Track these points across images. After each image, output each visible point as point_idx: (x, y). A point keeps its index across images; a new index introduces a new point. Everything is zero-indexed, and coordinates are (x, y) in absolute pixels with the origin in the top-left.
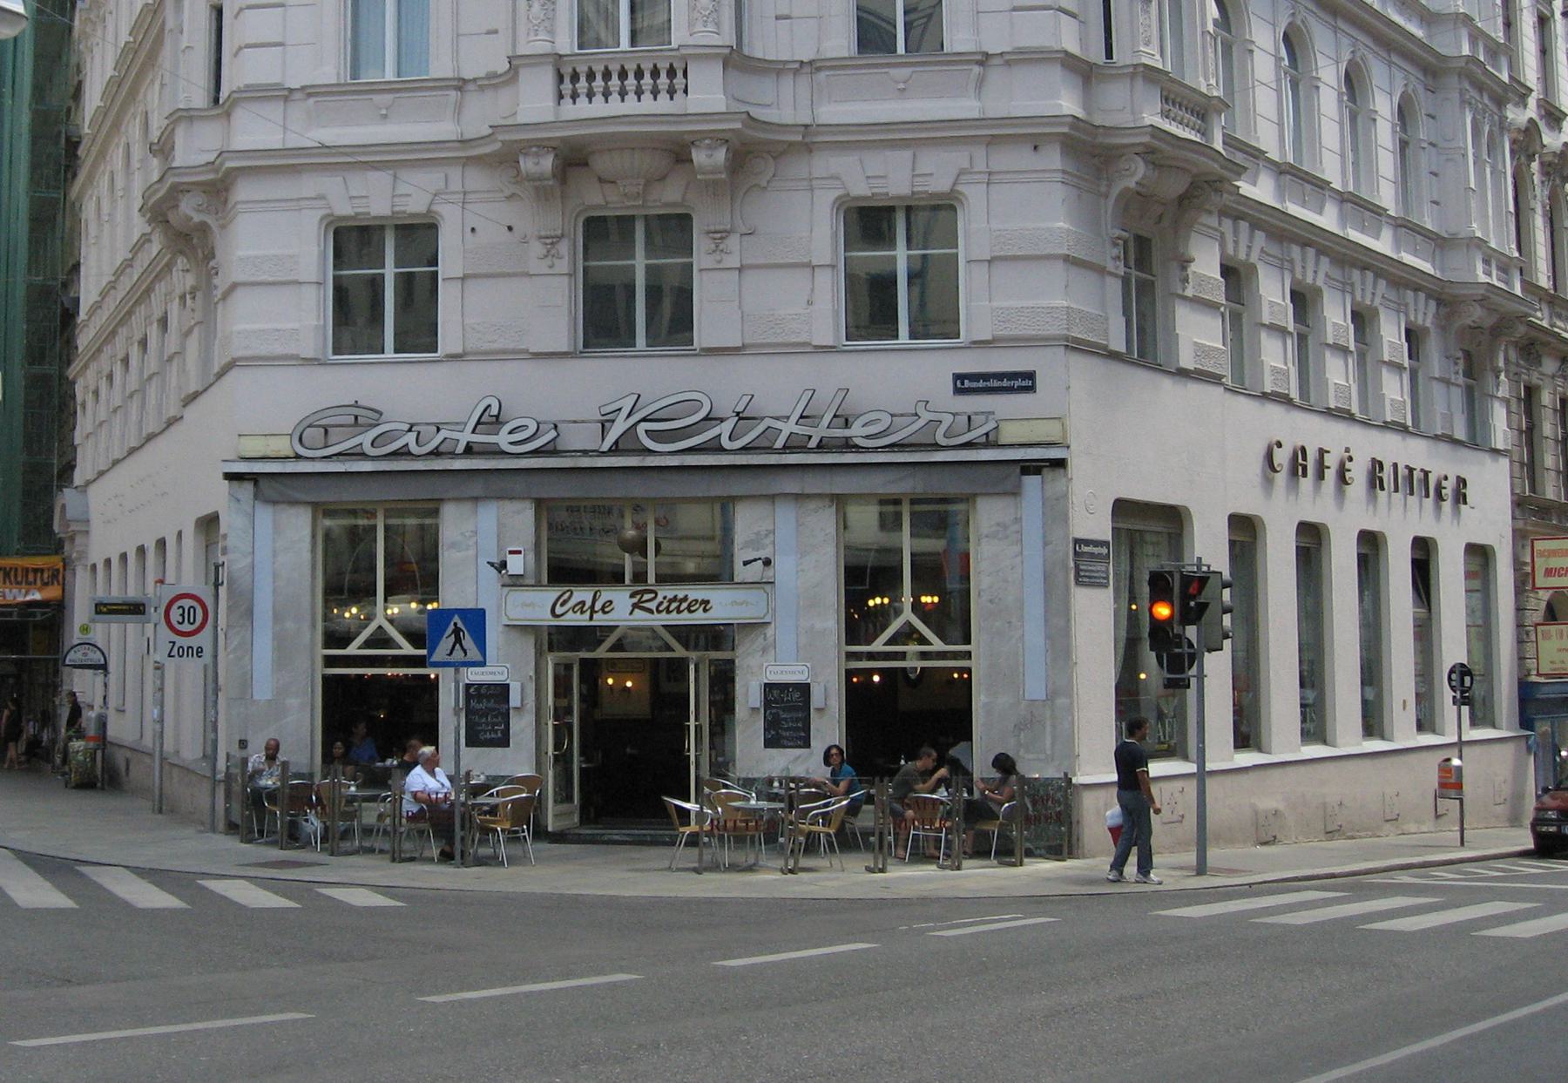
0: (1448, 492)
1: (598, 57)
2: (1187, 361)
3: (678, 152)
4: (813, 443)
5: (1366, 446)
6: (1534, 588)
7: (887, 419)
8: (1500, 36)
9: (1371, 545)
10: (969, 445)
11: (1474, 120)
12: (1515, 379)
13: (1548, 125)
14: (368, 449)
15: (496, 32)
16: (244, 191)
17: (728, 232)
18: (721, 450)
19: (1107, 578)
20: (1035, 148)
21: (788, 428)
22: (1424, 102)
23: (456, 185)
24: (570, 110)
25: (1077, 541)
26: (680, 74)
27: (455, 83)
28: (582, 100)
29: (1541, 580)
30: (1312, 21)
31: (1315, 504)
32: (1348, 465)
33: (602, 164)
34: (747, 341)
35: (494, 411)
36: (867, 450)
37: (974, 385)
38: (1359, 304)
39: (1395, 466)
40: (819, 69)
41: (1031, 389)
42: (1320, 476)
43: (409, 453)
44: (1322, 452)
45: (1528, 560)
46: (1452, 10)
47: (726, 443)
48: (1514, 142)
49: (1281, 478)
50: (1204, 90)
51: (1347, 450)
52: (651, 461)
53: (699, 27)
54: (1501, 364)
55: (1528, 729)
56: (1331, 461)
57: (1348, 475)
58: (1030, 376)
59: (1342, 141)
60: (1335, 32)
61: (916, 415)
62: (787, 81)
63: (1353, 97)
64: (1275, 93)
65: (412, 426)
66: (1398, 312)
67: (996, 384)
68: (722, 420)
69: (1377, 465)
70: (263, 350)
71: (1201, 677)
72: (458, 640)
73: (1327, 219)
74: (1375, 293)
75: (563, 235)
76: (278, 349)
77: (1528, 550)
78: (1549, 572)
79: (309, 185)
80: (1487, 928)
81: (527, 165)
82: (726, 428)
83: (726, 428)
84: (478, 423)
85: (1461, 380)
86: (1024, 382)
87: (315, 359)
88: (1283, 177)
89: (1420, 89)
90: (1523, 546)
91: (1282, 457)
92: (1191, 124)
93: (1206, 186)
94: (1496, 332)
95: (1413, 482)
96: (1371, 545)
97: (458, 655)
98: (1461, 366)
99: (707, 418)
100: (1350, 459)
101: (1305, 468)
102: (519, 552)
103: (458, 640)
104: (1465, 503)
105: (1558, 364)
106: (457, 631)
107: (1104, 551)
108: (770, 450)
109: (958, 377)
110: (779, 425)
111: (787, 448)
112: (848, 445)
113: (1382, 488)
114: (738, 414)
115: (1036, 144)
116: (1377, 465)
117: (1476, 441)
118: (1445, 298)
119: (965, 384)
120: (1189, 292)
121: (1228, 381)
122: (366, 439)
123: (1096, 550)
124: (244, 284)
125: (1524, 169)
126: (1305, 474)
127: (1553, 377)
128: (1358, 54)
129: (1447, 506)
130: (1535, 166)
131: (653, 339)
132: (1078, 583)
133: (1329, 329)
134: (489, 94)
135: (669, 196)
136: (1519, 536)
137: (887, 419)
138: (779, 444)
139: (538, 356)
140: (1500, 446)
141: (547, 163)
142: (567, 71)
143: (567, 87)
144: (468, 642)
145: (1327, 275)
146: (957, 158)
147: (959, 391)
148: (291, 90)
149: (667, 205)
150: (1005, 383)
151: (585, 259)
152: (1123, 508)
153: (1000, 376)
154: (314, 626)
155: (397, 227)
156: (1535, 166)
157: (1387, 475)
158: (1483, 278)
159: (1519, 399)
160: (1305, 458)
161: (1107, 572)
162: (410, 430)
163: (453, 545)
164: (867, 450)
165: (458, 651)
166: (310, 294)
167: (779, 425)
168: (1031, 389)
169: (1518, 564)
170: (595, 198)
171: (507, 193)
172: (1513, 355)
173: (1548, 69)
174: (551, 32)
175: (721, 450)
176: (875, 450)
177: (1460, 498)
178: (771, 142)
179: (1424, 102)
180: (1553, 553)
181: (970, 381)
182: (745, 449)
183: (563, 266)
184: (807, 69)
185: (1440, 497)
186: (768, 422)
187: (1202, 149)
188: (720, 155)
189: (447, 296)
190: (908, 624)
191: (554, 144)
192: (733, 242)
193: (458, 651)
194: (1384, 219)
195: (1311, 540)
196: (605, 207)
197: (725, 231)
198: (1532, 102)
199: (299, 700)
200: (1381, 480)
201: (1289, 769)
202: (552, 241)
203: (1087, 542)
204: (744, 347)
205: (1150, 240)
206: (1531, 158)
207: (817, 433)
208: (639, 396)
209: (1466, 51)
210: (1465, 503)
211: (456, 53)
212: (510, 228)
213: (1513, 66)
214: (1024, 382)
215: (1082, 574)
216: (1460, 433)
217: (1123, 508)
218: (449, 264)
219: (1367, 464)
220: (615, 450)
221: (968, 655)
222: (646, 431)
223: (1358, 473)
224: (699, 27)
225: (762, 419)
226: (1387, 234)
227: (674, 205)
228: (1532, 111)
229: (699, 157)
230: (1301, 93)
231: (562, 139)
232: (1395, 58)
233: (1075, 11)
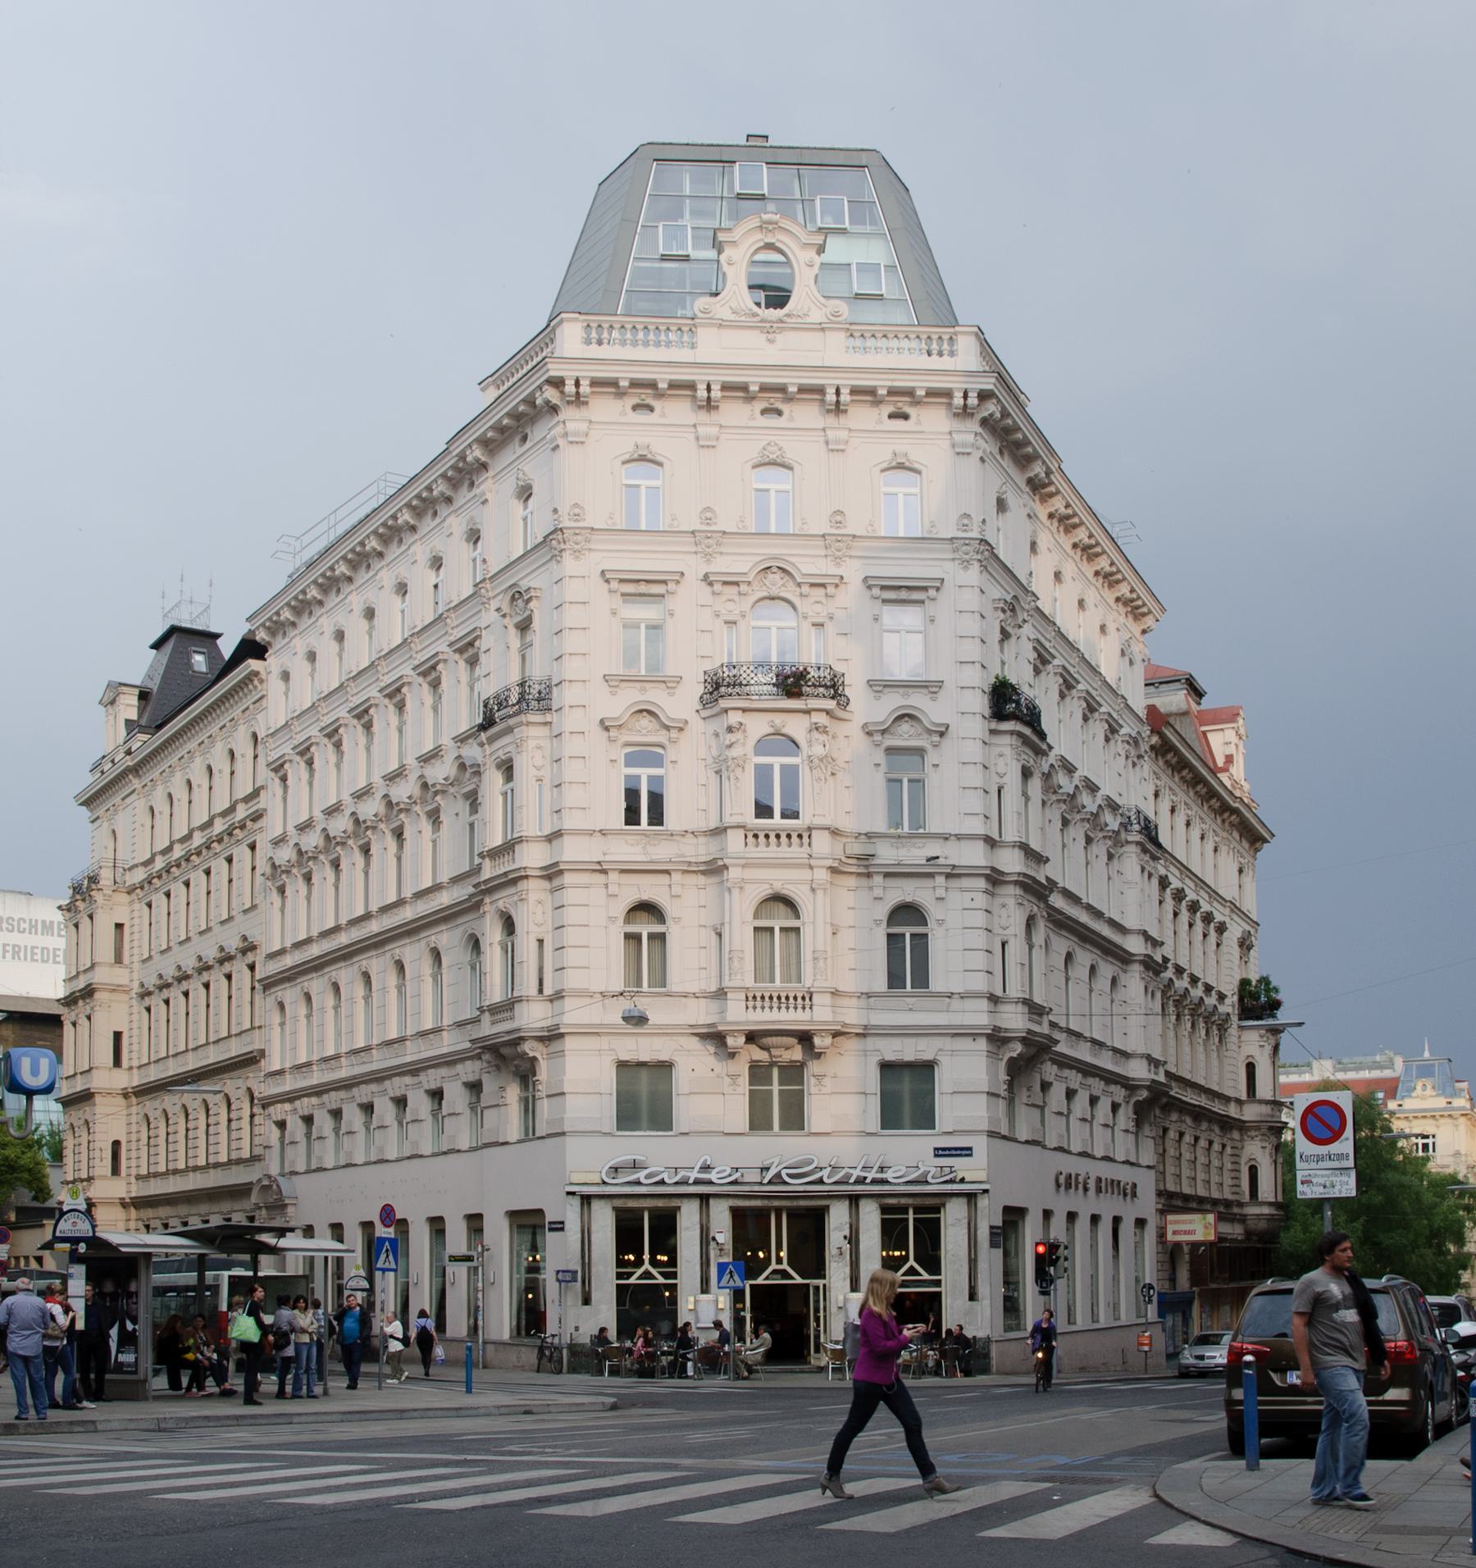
0: (1129, 1191)
1: (765, 987)
7: (904, 1169)
10: (951, 1181)
14: (643, 1180)
21: (856, 1173)
26: (807, 999)
36: (895, 1184)
41: (971, 1155)
42: (1077, 1188)
49: (1062, 1189)
56: (1081, 1179)
58: (970, 1149)
67: (954, 1152)
69: (1099, 1180)
71: (1055, 1290)
78: (1175, 1233)
80: (827, 1522)
91: (1062, 1179)
97: (387, 1265)
106: (731, 1272)
108: (847, 1183)
109: (936, 1149)
110: (851, 1171)
112: (884, 1182)
115: (974, 1036)
116: (1099, 1180)
119: (939, 1152)
122: (641, 1175)
129: (1129, 1198)
131: (782, 1128)
137: (904, 1169)
138: (852, 1181)
143: (751, 1004)
146: (938, 1043)
147: (936, 1156)
153: (950, 1149)
163: (687, 1228)
164: (895, 1184)
165: (732, 1282)
167: (851, 1171)
176: (899, 1184)
177: (1134, 1195)
182: (835, 1183)
185: (1125, 1195)
186: (846, 1170)
190: (912, 1267)
193: (732, 1282)
201: (1114, 1331)
202: (734, 1077)
207: (870, 1176)
220: (770, 1183)
221: (938, 1283)
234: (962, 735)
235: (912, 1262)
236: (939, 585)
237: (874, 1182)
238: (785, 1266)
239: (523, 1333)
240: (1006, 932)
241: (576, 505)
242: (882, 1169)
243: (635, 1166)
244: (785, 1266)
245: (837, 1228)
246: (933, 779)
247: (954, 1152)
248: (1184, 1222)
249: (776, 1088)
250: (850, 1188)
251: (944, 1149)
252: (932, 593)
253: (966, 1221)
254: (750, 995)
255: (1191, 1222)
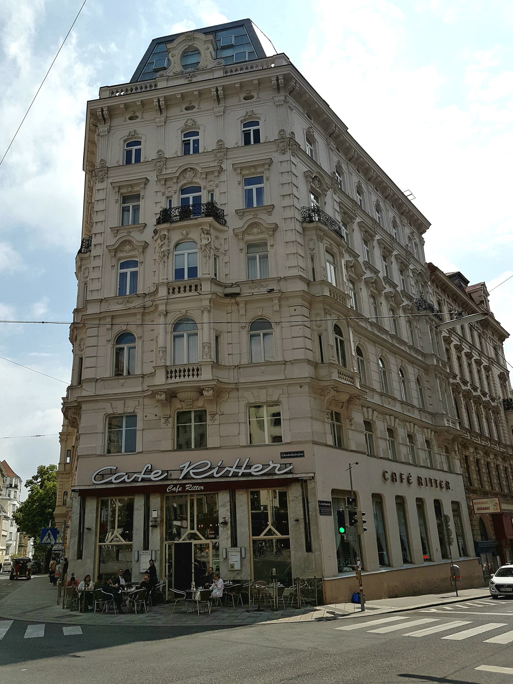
2: (353, 447)
3: (200, 391)
4: (240, 474)
5: (415, 472)
6: (475, 514)
8: (446, 360)
9: (420, 503)
11: (440, 382)
12: (461, 453)
13: (464, 384)
14: (114, 481)
15: (153, 362)
16: (84, 407)
17: (216, 414)
18: (214, 477)
19: (331, 513)
20: (301, 387)
21: (233, 470)
22: (424, 377)
23: (141, 403)
24: (170, 381)
25: (319, 502)
27: (141, 376)
28: (173, 378)
29: (476, 511)
30: (407, 365)
31: (401, 489)
32: (410, 478)
33: (181, 396)
34: (221, 445)
35: (150, 468)
37: (287, 455)
38: (366, 418)
39: (426, 478)
40: (240, 368)
41: (303, 456)
43: (126, 482)
44: (401, 475)
45: (472, 505)
46: (431, 353)
47: (215, 475)
48: (453, 389)
50: (352, 371)
51: (410, 474)
52: (195, 481)
53: (205, 357)
54: (457, 449)
55: (478, 557)
56: (405, 477)
57: (411, 481)
58: (302, 452)
59: (418, 395)
60: (396, 358)
61: (269, 465)
62: (231, 371)
63: (419, 385)
64: (416, 392)
65: (127, 473)
66: (422, 434)
67: (293, 455)
68: (214, 468)
70: (86, 453)
72: (49, 537)
73: (398, 408)
74: (410, 427)
75: (170, 417)
76: (90, 453)
77: (471, 502)
79: (100, 405)
81: (158, 397)
82: (215, 471)
83: (215, 471)
84: (145, 472)
85: (444, 454)
86: (300, 454)
87: (101, 455)
88: (382, 397)
89: (424, 374)
90: (470, 502)
91: (388, 476)
92: (347, 379)
93: (355, 397)
94: (454, 440)
95: (431, 482)
96: (420, 503)
98: (444, 450)
99: (210, 468)
100: (411, 476)
101: (396, 479)
102: (156, 510)
103: (49, 537)
104: (450, 489)
105: (474, 449)
106: (49, 534)
107: (329, 504)
108: (228, 477)
111: (233, 476)
112: (250, 475)
113: (422, 485)
114: (219, 466)
117: (451, 471)
118: (437, 431)
119: (284, 455)
120: (353, 428)
121: (367, 453)
123: (326, 504)
124: (82, 434)
125: (458, 396)
126: (396, 481)
127: (473, 453)
128: (403, 364)
130: (461, 395)
132: (321, 515)
133: (379, 432)
134: (150, 378)
135: (200, 404)
136: (468, 498)
138: (230, 475)
139: (162, 451)
140: (459, 473)
141: (163, 397)
142: (169, 370)
143: (169, 375)
144: (52, 537)
145: (398, 424)
148: (97, 379)
149: (199, 407)
150: (295, 455)
151: (177, 424)
152: (334, 491)
154: (96, 535)
155: (127, 417)
156: (461, 395)
157: (423, 481)
158: (447, 425)
159: (463, 459)
160: (396, 476)
161: (331, 511)
162: (126, 475)
166: (100, 436)
167: (230, 469)
168: (303, 456)
169: (469, 507)
170: (178, 406)
171: (155, 405)
172: (460, 446)
173: (482, 383)
174: (165, 360)
175: (214, 477)
177: (448, 488)
178: (226, 388)
179: (424, 377)
180: (479, 503)
181: (285, 454)
182: (221, 477)
183: (170, 425)
184: (237, 368)
185: (441, 488)
186: (227, 468)
187: (353, 387)
188: (211, 392)
189: (139, 435)
191: (166, 390)
192: (217, 416)
194: (415, 409)
195: (401, 501)
196: (182, 408)
197: (215, 414)
198: (479, 390)
199: (31, 558)
200: (422, 483)
202: (167, 418)
203: (323, 502)
204: (220, 447)
205: (340, 413)
206: (459, 393)
208: (191, 462)
209: (435, 363)
210: (450, 489)
211: (142, 369)
212: (156, 415)
213: (451, 368)
214: (300, 454)
215: (139, 503)
216: (446, 469)
217: (334, 491)
218: (140, 425)
219: (416, 478)
222: (193, 473)
223: (414, 480)
224: (205, 357)
225: (225, 467)
226: (416, 412)
227: (201, 407)
228: (458, 380)
229: (205, 393)
230: (406, 384)
231: (168, 389)
232: (415, 366)
233: (311, 349)
234: (284, 229)
235: (270, 526)
236: (271, 162)
237: (244, 475)
238: (195, 531)
239: (462, 555)
240: (320, 329)
241: (102, 160)
242: (249, 467)
243: (112, 473)
244: (195, 531)
245: (224, 506)
246: (271, 252)
247: (293, 455)
248: (482, 503)
249: (193, 424)
250: (228, 479)
251: (286, 453)
252: (267, 167)
253: (301, 498)
254: (169, 370)
255: (486, 503)
